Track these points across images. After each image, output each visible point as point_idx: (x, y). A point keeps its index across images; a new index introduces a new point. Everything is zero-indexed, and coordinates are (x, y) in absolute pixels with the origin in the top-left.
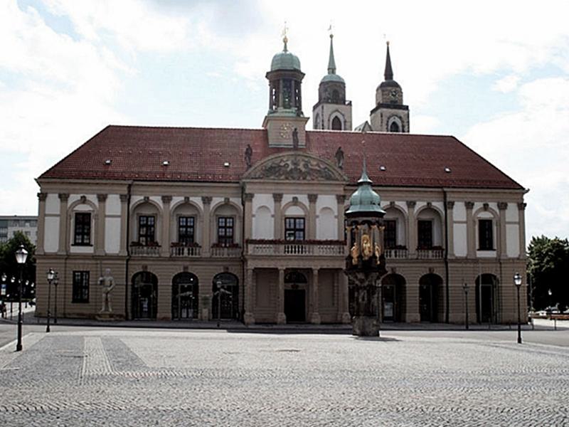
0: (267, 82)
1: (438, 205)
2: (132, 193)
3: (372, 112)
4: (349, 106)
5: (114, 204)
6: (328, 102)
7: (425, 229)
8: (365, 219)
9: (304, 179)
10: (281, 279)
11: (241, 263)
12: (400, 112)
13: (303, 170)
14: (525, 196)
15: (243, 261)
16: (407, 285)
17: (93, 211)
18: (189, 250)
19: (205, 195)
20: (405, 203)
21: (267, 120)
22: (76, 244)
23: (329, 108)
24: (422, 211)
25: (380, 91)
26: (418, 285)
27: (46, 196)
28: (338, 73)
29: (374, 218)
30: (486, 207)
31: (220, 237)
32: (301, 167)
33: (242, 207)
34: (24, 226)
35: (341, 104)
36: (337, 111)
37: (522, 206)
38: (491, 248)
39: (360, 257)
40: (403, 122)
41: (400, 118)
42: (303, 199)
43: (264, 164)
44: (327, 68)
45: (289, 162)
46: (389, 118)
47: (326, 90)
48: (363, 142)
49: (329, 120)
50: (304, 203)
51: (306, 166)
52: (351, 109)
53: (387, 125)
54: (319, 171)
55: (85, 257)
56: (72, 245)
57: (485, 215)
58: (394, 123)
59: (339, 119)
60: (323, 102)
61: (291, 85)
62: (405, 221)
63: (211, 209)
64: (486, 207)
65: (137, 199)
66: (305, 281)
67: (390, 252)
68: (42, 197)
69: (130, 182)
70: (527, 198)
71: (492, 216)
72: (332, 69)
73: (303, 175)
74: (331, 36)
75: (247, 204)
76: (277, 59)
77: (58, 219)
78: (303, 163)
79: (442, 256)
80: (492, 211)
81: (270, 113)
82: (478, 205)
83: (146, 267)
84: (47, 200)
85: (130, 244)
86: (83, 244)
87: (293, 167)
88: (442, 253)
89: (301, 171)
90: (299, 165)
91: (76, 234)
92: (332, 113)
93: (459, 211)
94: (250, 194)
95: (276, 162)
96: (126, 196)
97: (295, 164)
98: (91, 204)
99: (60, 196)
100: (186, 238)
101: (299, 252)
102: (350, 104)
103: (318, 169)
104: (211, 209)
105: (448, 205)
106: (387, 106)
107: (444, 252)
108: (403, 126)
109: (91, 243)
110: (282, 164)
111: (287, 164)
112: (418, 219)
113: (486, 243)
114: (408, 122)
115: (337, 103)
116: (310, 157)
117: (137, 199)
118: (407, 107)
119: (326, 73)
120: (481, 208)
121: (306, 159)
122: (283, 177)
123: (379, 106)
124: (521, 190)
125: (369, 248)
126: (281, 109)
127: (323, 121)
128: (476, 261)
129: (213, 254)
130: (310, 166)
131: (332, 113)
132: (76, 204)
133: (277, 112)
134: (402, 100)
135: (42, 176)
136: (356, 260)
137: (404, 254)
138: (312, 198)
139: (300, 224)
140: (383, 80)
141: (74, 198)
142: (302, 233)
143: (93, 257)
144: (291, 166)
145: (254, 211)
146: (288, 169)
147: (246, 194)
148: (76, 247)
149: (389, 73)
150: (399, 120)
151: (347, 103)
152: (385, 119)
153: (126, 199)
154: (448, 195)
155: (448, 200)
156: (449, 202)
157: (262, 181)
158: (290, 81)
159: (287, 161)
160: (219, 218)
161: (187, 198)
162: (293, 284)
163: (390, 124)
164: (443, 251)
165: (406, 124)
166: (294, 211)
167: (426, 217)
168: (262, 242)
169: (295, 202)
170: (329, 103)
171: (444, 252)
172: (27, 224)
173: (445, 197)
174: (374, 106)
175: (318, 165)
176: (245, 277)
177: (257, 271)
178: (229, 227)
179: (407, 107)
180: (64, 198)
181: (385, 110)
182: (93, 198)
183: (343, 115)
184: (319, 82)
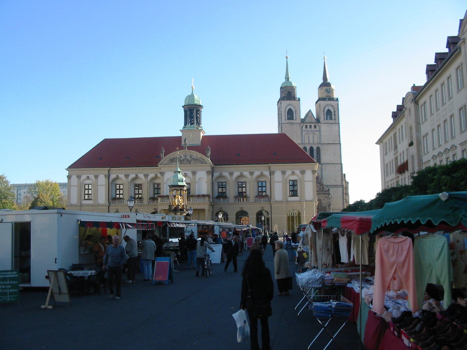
0: (183, 109)
4: (299, 101)
6: (284, 100)
9: (190, 163)
12: (332, 102)
13: (189, 159)
19: (145, 173)
20: (248, 173)
23: (285, 103)
25: (319, 89)
26: (256, 216)
27: (71, 177)
28: (290, 80)
30: (293, 173)
31: (239, 193)
32: (188, 157)
35: (293, 100)
38: (297, 196)
40: (334, 109)
41: (333, 106)
43: (169, 157)
44: (284, 78)
46: (325, 107)
48: (178, 153)
49: (285, 111)
51: (191, 157)
52: (300, 103)
53: (324, 111)
56: (83, 200)
57: (293, 178)
59: (292, 110)
64: (293, 173)
65: (113, 176)
68: (69, 177)
71: (298, 178)
72: (287, 78)
73: (189, 162)
74: (287, 58)
77: (77, 187)
78: (189, 155)
80: (297, 175)
81: (184, 128)
82: (289, 172)
84: (72, 178)
89: (188, 160)
90: (187, 157)
91: (297, 191)
92: (288, 106)
93: (278, 176)
96: (107, 175)
97: (186, 156)
99: (77, 177)
100: (241, 195)
101: (163, 201)
102: (299, 99)
103: (197, 158)
104: (148, 179)
106: (324, 99)
108: (335, 112)
113: (294, 193)
114: (338, 109)
115: (290, 100)
119: (284, 80)
120: (291, 174)
121: (191, 154)
123: (320, 99)
130: (193, 157)
131: (288, 106)
132: (84, 180)
134: (333, 97)
135: (69, 167)
138: (194, 173)
139: (264, 184)
142: (225, 189)
144: (183, 157)
146: (182, 159)
148: (85, 201)
150: (331, 107)
152: (322, 108)
154: (271, 168)
155: (272, 170)
156: (272, 172)
161: (137, 175)
163: (326, 110)
164: (268, 198)
165: (336, 110)
170: (285, 100)
173: (270, 169)
178: (260, 187)
180: (79, 177)
181: (322, 102)
183: (295, 107)
184: (280, 88)
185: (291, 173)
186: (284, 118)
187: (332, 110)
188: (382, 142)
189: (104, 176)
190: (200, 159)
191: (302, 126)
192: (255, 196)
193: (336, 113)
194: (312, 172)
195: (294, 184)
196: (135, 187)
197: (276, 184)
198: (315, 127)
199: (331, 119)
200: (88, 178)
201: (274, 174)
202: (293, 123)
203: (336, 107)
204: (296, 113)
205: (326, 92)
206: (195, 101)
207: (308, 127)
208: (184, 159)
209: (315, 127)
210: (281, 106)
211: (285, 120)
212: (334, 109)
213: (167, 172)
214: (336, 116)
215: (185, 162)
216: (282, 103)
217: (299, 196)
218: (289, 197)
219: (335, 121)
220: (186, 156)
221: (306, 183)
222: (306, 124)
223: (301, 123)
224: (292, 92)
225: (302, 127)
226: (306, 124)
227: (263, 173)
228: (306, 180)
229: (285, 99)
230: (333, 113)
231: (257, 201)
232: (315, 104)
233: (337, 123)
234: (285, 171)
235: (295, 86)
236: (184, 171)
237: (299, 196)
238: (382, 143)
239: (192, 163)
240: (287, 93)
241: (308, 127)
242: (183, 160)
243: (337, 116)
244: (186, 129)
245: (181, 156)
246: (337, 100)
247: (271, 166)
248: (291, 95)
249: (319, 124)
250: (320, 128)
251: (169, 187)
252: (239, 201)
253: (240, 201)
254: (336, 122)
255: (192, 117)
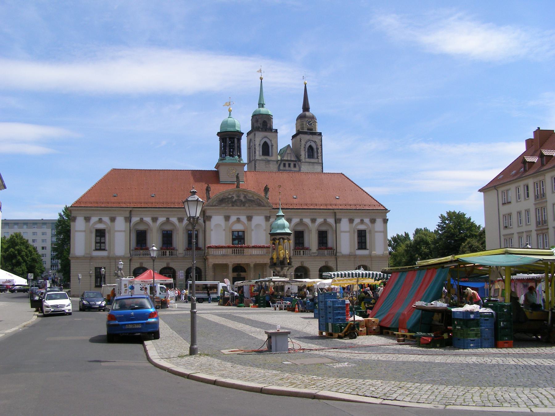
1: (331, 221)
2: (132, 215)
3: (294, 137)
5: (120, 223)
7: (323, 236)
8: (281, 236)
10: (230, 270)
11: (204, 260)
12: (316, 138)
13: (243, 200)
14: (388, 214)
15: (205, 260)
16: (311, 273)
17: (107, 228)
18: (170, 252)
19: (180, 216)
21: (217, 166)
22: (96, 250)
24: (321, 225)
29: (286, 236)
30: (362, 221)
32: (242, 198)
33: (203, 224)
34: (22, 228)
36: (266, 137)
37: (386, 221)
38: (365, 248)
39: (278, 258)
41: (315, 142)
42: (243, 218)
44: (258, 104)
45: (234, 195)
46: (306, 143)
47: (257, 121)
50: (245, 222)
51: (245, 197)
54: (253, 200)
55: (103, 258)
57: (362, 227)
58: (311, 147)
60: (255, 130)
61: (234, 141)
62: (310, 231)
63: (184, 225)
64: (100, 221)
65: (135, 219)
66: (245, 271)
67: (300, 252)
69: (131, 209)
70: (389, 216)
74: (261, 79)
75: (207, 223)
76: (224, 124)
78: (243, 195)
79: (333, 254)
80: (366, 224)
81: (220, 160)
82: (357, 221)
83: (142, 263)
85: (131, 249)
86: (100, 249)
87: (237, 198)
88: (333, 251)
89: (242, 201)
94: (209, 216)
95: (226, 195)
97: (238, 196)
98: (105, 223)
103: (253, 199)
105: (337, 221)
107: (335, 252)
108: (317, 149)
109: (106, 249)
110: (230, 196)
111: (233, 197)
112: (317, 229)
114: (322, 145)
116: (248, 192)
117: (135, 219)
118: (321, 133)
120: (359, 223)
121: (245, 194)
122: (230, 205)
123: (299, 133)
124: (386, 211)
125: (283, 253)
126: (228, 157)
127: (255, 145)
128: (92, 258)
129: (185, 255)
132: (95, 223)
133: (225, 159)
136: (276, 260)
137: (309, 253)
138: (250, 218)
140: (301, 111)
141: (94, 219)
143: (108, 258)
144: (235, 198)
145: (212, 227)
146: (234, 200)
147: (206, 216)
149: (306, 108)
150: (314, 143)
151: (273, 131)
152: (303, 142)
153: (128, 219)
154: (337, 214)
155: (337, 217)
156: (338, 219)
157: (217, 207)
158: (234, 138)
159: (233, 194)
160: (188, 231)
161: (168, 219)
162: (238, 273)
163: (307, 146)
165: (319, 147)
166: (238, 227)
167: (323, 228)
168: (217, 247)
169: (238, 220)
171: (335, 252)
172: (16, 226)
173: (335, 215)
174: (294, 132)
175: (253, 197)
176: (207, 269)
177: (215, 266)
179: (321, 133)
182: (106, 219)
185: (360, 221)
186: (258, 154)
187: (314, 147)
188: (497, 190)
189: (310, 220)
190: (258, 200)
191: (279, 164)
192: (184, 249)
193: (319, 151)
194: (349, 221)
195: (101, 233)
196: (188, 232)
197: (342, 234)
198: (295, 166)
199: (313, 158)
200: (100, 221)
201: (340, 223)
202: (269, 161)
203: (319, 144)
204: (272, 148)
205: (307, 124)
206: (236, 128)
207: (287, 165)
208: (236, 199)
209: (295, 166)
210: (255, 137)
211: (260, 156)
212: (317, 145)
213: (214, 216)
214: (319, 154)
215: (238, 204)
216: (256, 135)
217: (368, 249)
218: (357, 249)
219: (317, 159)
220: (238, 196)
221: (117, 234)
222: (284, 162)
223: (300, 161)
224: (268, 122)
225: (280, 165)
226: (284, 162)
227: (326, 221)
228: (117, 229)
229: (260, 129)
230: (315, 150)
231: (298, 255)
232: (246, 136)
233: (320, 163)
234: (353, 219)
235: (271, 115)
236: (238, 216)
237: (368, 248)
238: (496, 191)
239: (247, 205)
240: (262, 122)
241: (287, 165)
242: (235, 201)
243: (319, 154)
244: (224, 161)
245: (233, 195)
246: (320, 134)
247: (336, 213)
248: (267, 125)
249: (299, 163)
250: (300, 168)
251: (270, 235)
252: (299, 255)
253: (300, 254)
254: (318, 161)
255: (232, 147)
